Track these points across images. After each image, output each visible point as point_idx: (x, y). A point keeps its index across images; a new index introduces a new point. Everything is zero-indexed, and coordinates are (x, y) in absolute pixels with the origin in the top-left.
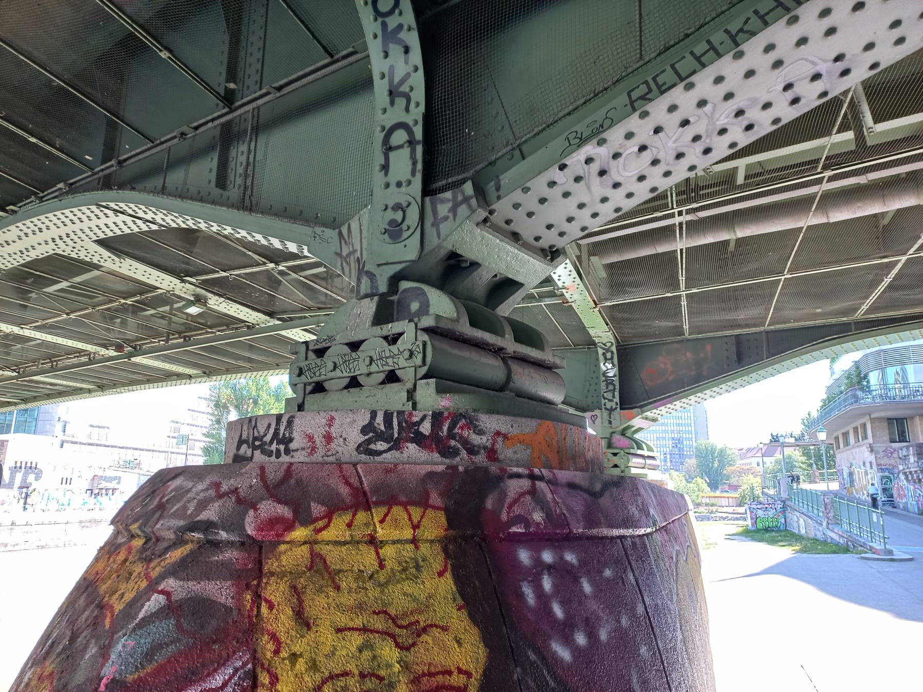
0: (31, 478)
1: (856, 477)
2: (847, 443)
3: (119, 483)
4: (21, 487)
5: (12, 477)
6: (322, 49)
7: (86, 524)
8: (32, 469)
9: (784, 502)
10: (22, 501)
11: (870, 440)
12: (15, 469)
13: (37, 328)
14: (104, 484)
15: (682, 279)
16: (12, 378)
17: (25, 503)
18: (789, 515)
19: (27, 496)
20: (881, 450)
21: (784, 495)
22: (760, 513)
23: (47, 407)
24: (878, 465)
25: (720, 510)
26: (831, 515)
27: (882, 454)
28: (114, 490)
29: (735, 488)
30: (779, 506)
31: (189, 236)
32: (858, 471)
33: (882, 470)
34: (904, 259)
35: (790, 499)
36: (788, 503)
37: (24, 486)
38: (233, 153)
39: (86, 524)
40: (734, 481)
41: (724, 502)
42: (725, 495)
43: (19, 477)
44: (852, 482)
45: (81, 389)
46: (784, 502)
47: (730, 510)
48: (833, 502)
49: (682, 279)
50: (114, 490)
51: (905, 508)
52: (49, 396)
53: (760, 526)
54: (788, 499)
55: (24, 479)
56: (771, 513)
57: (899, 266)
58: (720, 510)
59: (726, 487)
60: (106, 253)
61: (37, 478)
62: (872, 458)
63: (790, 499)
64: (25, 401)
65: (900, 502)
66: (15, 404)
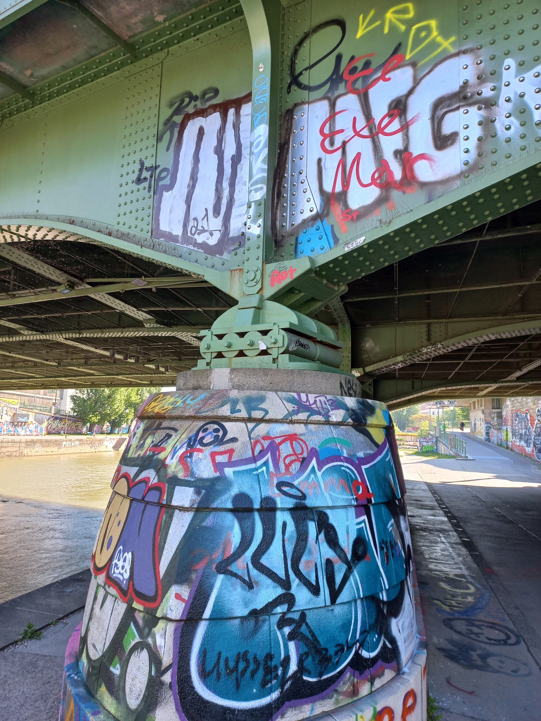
1: (477, 426)
2: (474, 408)
3: (28, 419)
6: (534, 661)
7: (29, 443)
9: (437, 438)
11: (483, 408)
14: (20, 419)
15: (439, 50)
18: (438, 445)
20: (487, 413)
21: (438, 435)
22: (425, 444)
24: (485, 420)
25: (405, 443)
26: (452, 444)
27: (488, 415)
28: (25, 423)
29: (416, 429)
30: (434, 440)
32: (478, 423)
33: (487, 423)
34: (463, 362)
35: (440, 437)
36: (439, 439)
39: (29, 443)
40: (416, 425)
41: (408, 438)
42: (409, 434)
44: (475, 428)
46: (437, 438)
47: (412, 443)
48: (454, 438)
49: (439, 50)
51: (493, 443)
53: (424, 450)
54: (439, 437)
56: (430, 444)
57: (461, 364)
58: (405, 443)
59: (411, 429)
62: (482, 416)
63: (440, 437)
65: (492, 439)
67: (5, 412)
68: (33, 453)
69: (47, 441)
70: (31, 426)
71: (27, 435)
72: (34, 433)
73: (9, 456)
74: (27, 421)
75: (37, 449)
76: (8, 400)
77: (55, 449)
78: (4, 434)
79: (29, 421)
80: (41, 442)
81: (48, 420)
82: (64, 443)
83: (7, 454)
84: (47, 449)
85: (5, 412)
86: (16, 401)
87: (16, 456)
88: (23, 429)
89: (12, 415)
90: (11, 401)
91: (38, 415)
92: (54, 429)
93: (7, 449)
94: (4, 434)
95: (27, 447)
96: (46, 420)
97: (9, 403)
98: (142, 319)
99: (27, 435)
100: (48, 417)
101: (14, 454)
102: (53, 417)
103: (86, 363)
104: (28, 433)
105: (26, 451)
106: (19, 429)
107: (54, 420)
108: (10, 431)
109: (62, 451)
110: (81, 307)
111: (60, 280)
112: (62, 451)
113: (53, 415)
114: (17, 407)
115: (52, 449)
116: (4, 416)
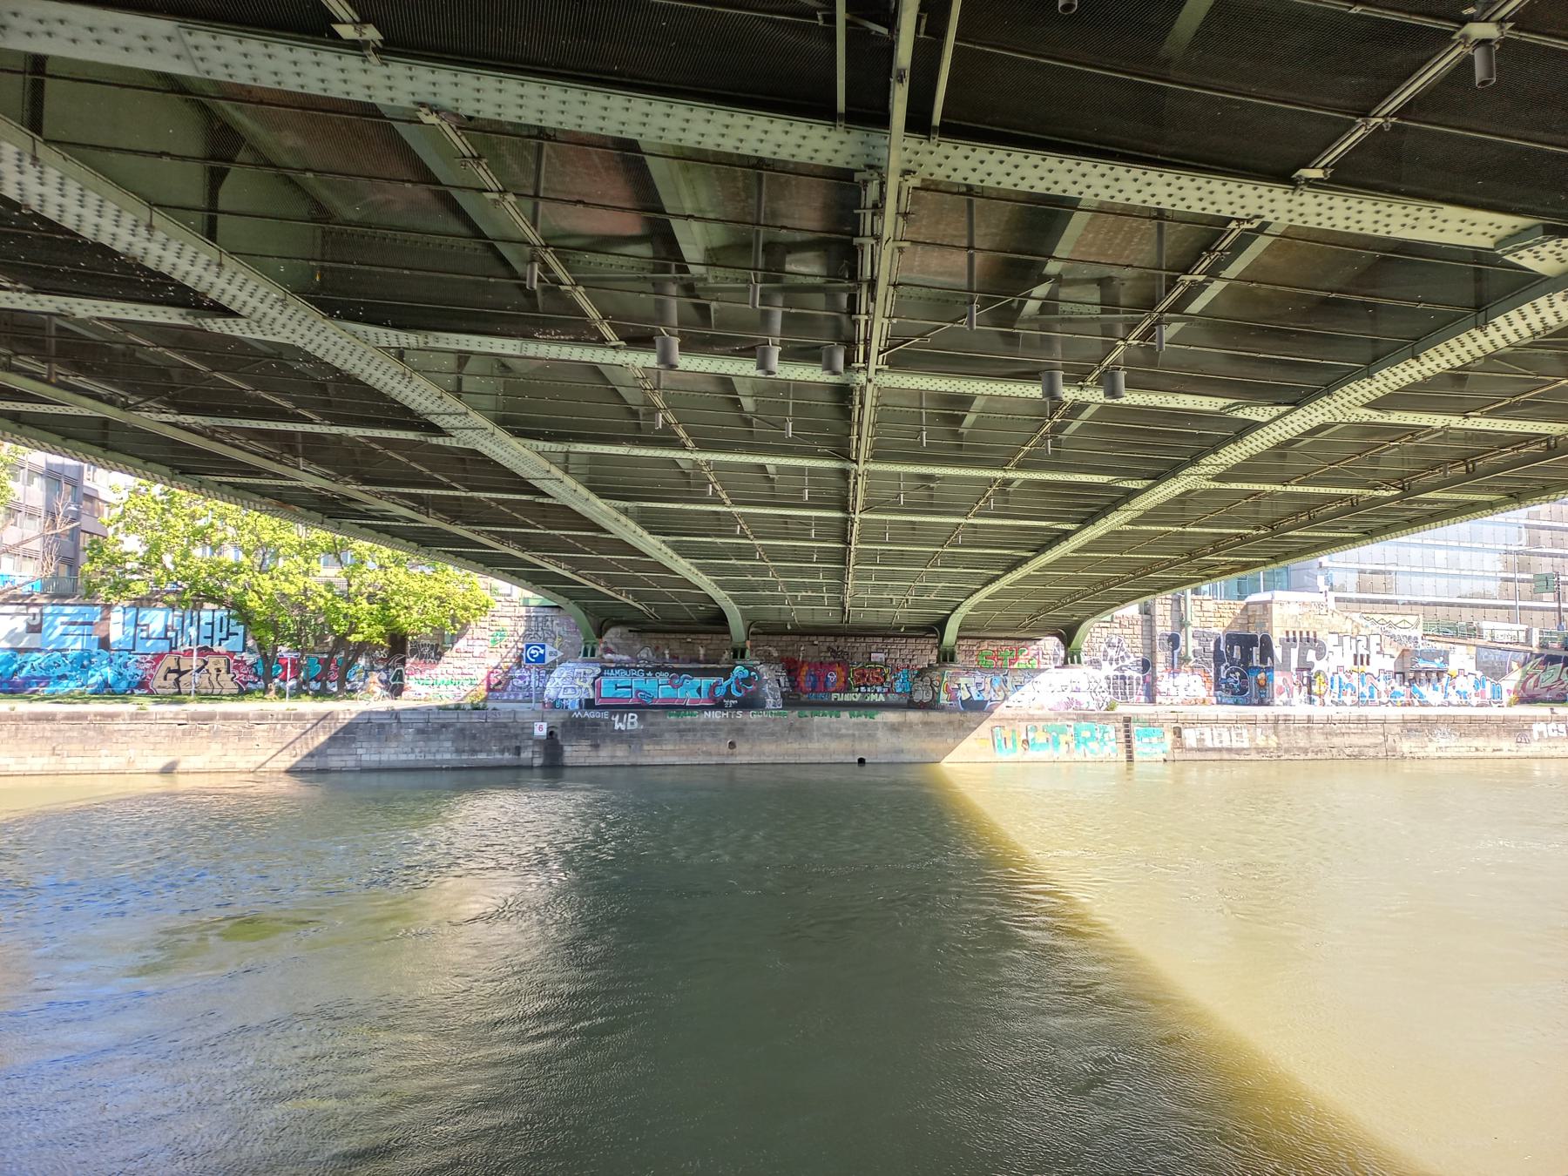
0: (1311, 656)
3: (1446, 661)
4: (1299, 669)
5: (1286, 655)
8: (1310, 641)
10: (1305, 689)
12: (1288, 642)
13: (1299, 484)
14: (1422, 664)
16: (1393, 498)
17: (1310, 692)
19: (1310, 682)
23: (1294, 564)
28: (1440, 673)
31: (105, 422)
37: (1305, 667)
38: (810, 255)
43: (1294, 653)
45: (1342, 539)
50: (1440, 673)
52: (1301, 552)
55: (1302, 657)
60: (1374, 413)
61: (1319, 657)
64: (1275, 559)
66: (1265, 564)
67: (1374, 648)
68: (1431, 749)
69: (1471, 720)
70: (1460, 681)
71: (1450, 704)
72: (1475, 700)
73: (1356, 757)
74: (1443, 667)
75: (1443, 742)
76: (1387, 618)
77: (1507, 745)
78: (1381, 703)
79: (1452, 668)
80: (1453, 722)
81: (1524, 664)
82: (1537, 727)
83: (1348, 751)
84: (1479, 742)
85: (1374, 648)
86: (1412, 619)
87: (1376, 758)
88: (1435, 689)
89: (1397, 654)
90: (1396, 619)
91: (1484, 653)
92: (1549, 688)
93: (1347, 740)
94: (1381, 703)
95: (1408, 737)
96: (1515, 666)
97: (1390, 624)
98: (1487, 243)
99: (1450, 704)
100: (1522, 657)
101: (1372, 752)
102: (1538, 656)
103: (1471, 474)
104: (1454, 699)
105: (1406, 746)
106: (1425, 690)
107: (1544, 663)
108: (1395, 695)
109: (1526, 750)
110: (1376, 291)
111: (346, 17)
112: (1526, 750)
113: (1537, 651)
114: (1419, 633)
115: (1494, 742)
116: (1374, 658)
